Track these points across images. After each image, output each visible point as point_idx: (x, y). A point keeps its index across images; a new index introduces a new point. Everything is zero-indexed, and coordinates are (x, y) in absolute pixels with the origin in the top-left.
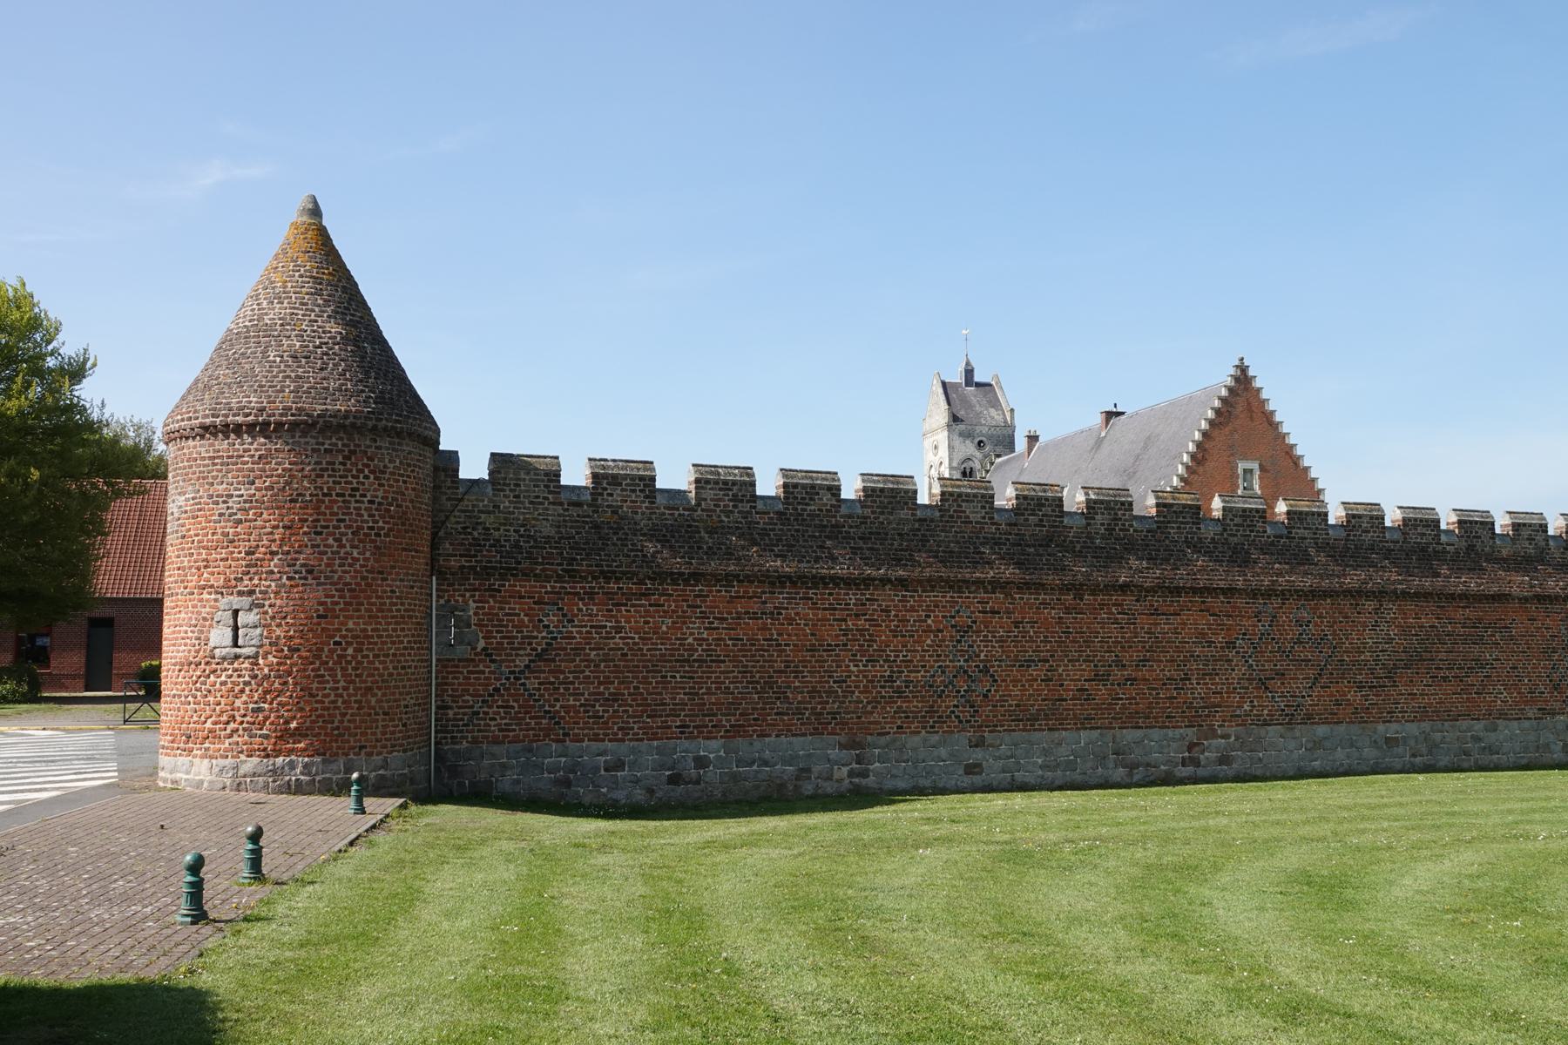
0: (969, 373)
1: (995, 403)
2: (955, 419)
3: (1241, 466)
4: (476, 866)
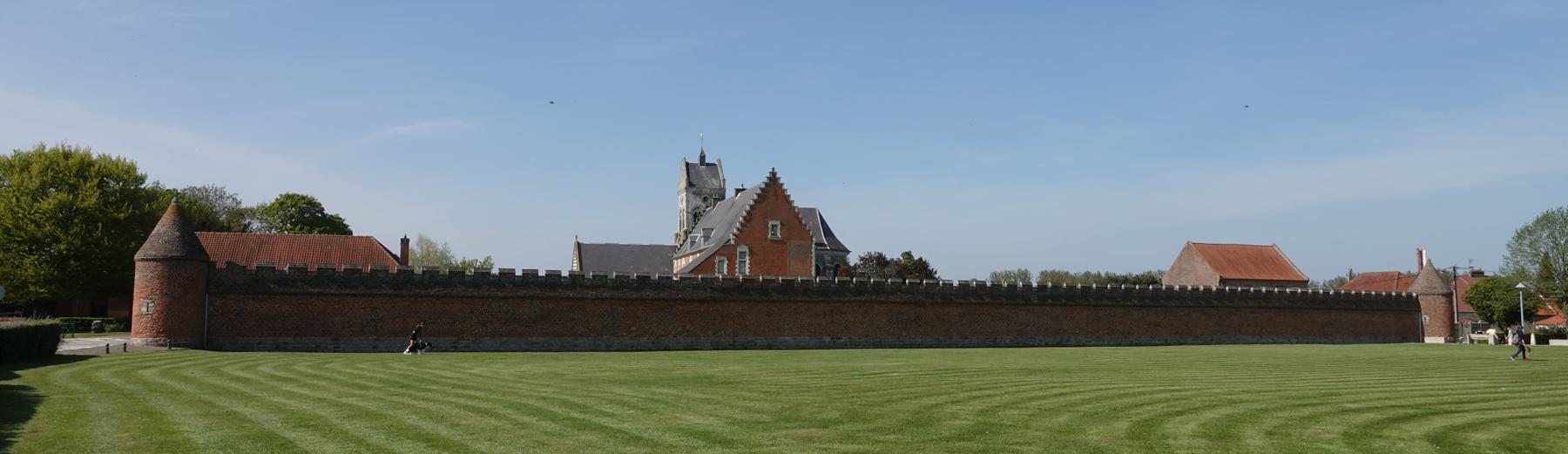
0: (702, 158)
1: (716, 176)
2: (690, 184)
3: (771, 223)
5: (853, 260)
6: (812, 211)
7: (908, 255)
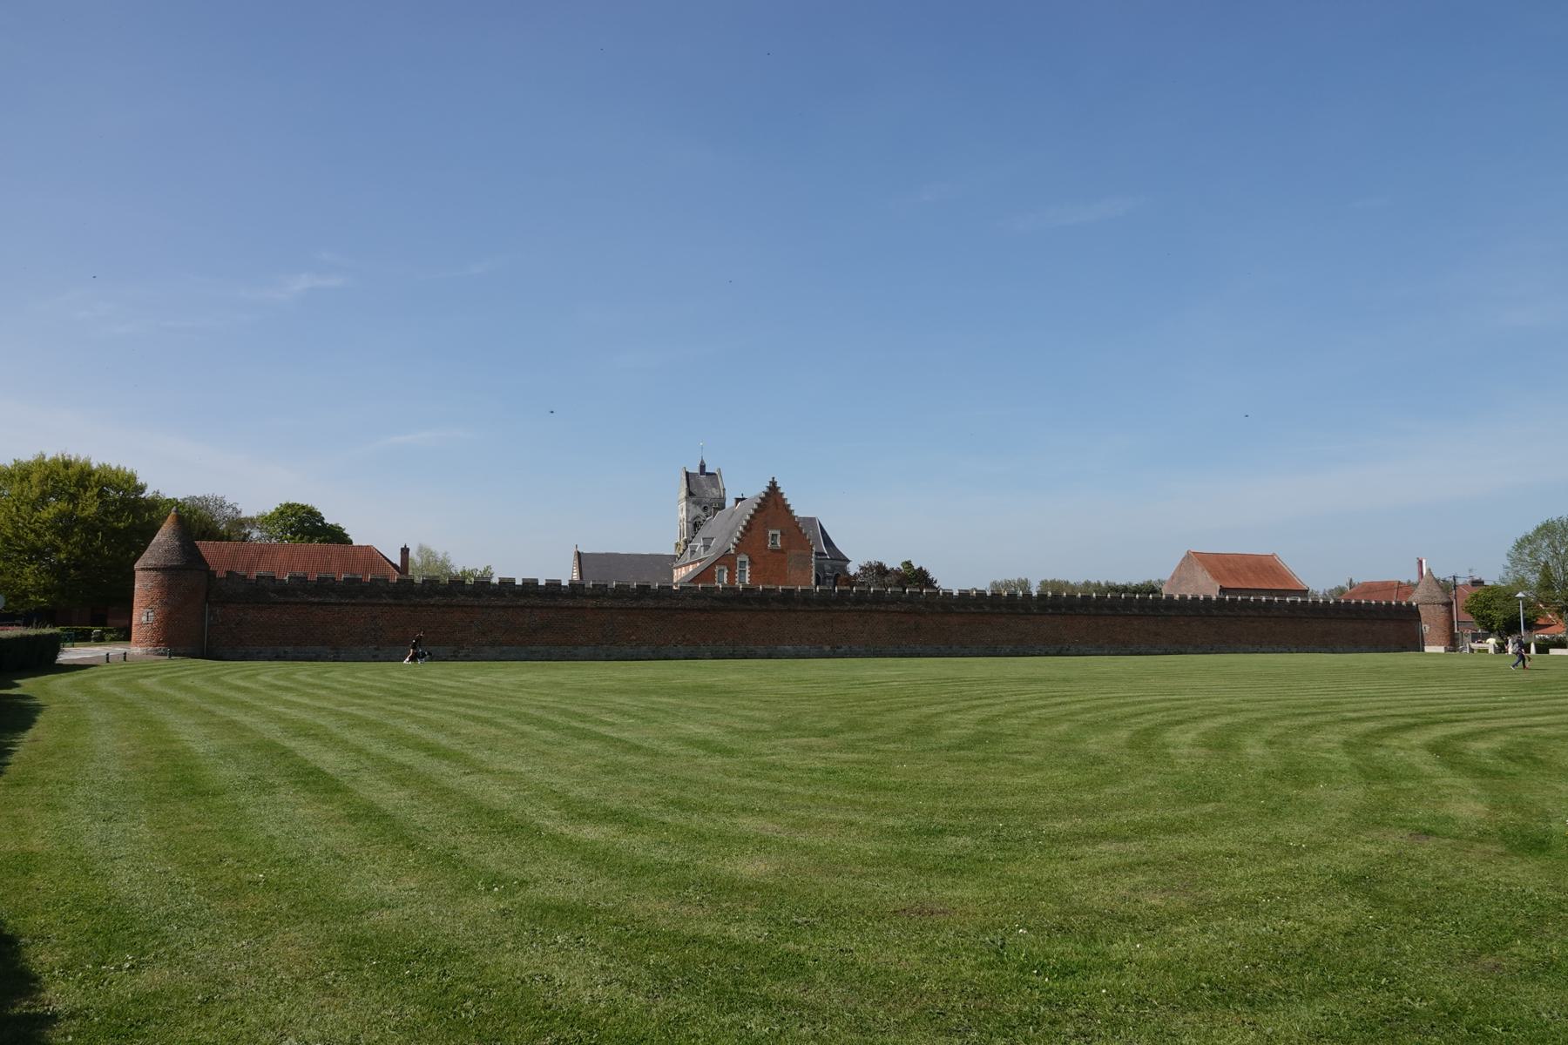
0: (702, 467)
1: (716, 485)
2: (690, 494)
4: (197, 673)
5: (853, 569)
6: (812, 520)
7: (908, 564)
